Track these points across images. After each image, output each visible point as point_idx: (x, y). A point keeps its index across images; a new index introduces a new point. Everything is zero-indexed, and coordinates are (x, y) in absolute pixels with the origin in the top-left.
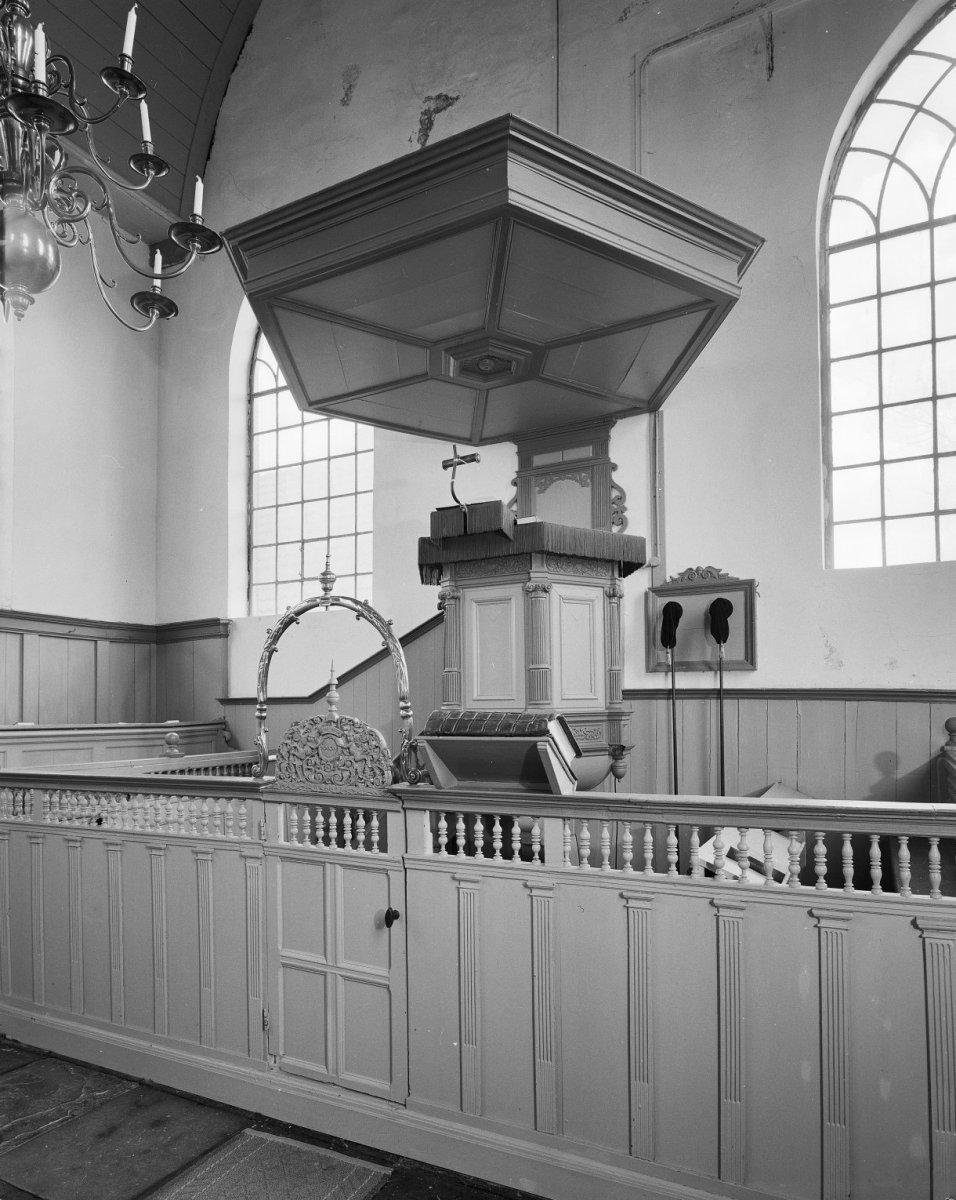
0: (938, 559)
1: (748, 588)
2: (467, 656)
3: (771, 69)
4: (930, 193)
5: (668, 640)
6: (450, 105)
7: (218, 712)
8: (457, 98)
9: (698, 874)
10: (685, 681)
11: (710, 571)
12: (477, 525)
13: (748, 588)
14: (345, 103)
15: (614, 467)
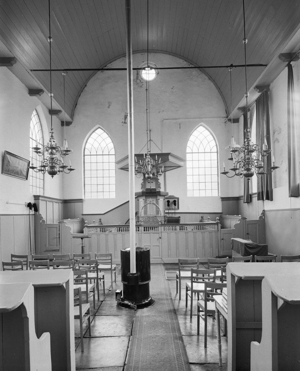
0: (187, 153)
1: (178, 199)
2: (240, 204)
3: (180, 128)
7: (82, 216)
11: (173, 196)
12: (153, 191)
13: (178, 199)
14: (109, 107)
15: (159, 179)
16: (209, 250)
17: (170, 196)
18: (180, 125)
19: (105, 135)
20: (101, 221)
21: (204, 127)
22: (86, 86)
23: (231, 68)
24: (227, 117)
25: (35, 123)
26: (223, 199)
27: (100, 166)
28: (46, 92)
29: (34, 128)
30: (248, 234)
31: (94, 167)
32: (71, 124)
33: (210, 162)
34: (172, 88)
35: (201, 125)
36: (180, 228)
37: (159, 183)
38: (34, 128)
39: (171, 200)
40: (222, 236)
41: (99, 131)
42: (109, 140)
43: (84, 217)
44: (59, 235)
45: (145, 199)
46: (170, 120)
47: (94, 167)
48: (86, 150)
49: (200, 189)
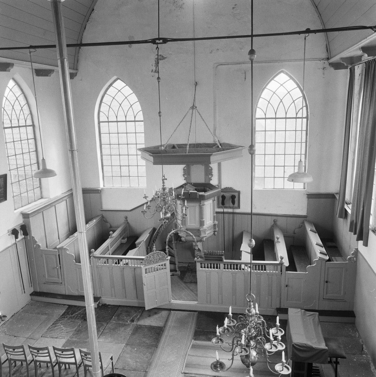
1: (239, 193)
3: (245, 78)
4: (276, 111)
5: (223, 203)
6: (164, 59)
7: (101, 213)
8: (166, 58)
9: (242, 270)
10: (226, 210)
11: (231, 188)
13: (239, 193)
16: (267, 298)
17: (226, 188)
18: (245, 73)
19: (128, 90)
20: (127, 220)
21: (287, 74)
22: (93, 10)
23: (307, 35)
24: (328, 59)
25: (12, 98)
26: (310, 196)
27: (123, 140)
28: (16, 63)
29: (13, 108)
30: (327, 282)
31: (114, 140)
32: (76, 75)
33: (275, 175)
34: (233, 8)
35: (282, 72)
36: (225, 267)
37: (210, 168)
38: (13, 108)
39: (228, 195)
40: (287, 282)
41: (119, 84)
42: (134, 98)
43: (104, 214)
44: (60, 264)
45: (182, 204)
46: (230, 66)
47: (114, 140)
48: (101, 113)
49: (275, 176)
